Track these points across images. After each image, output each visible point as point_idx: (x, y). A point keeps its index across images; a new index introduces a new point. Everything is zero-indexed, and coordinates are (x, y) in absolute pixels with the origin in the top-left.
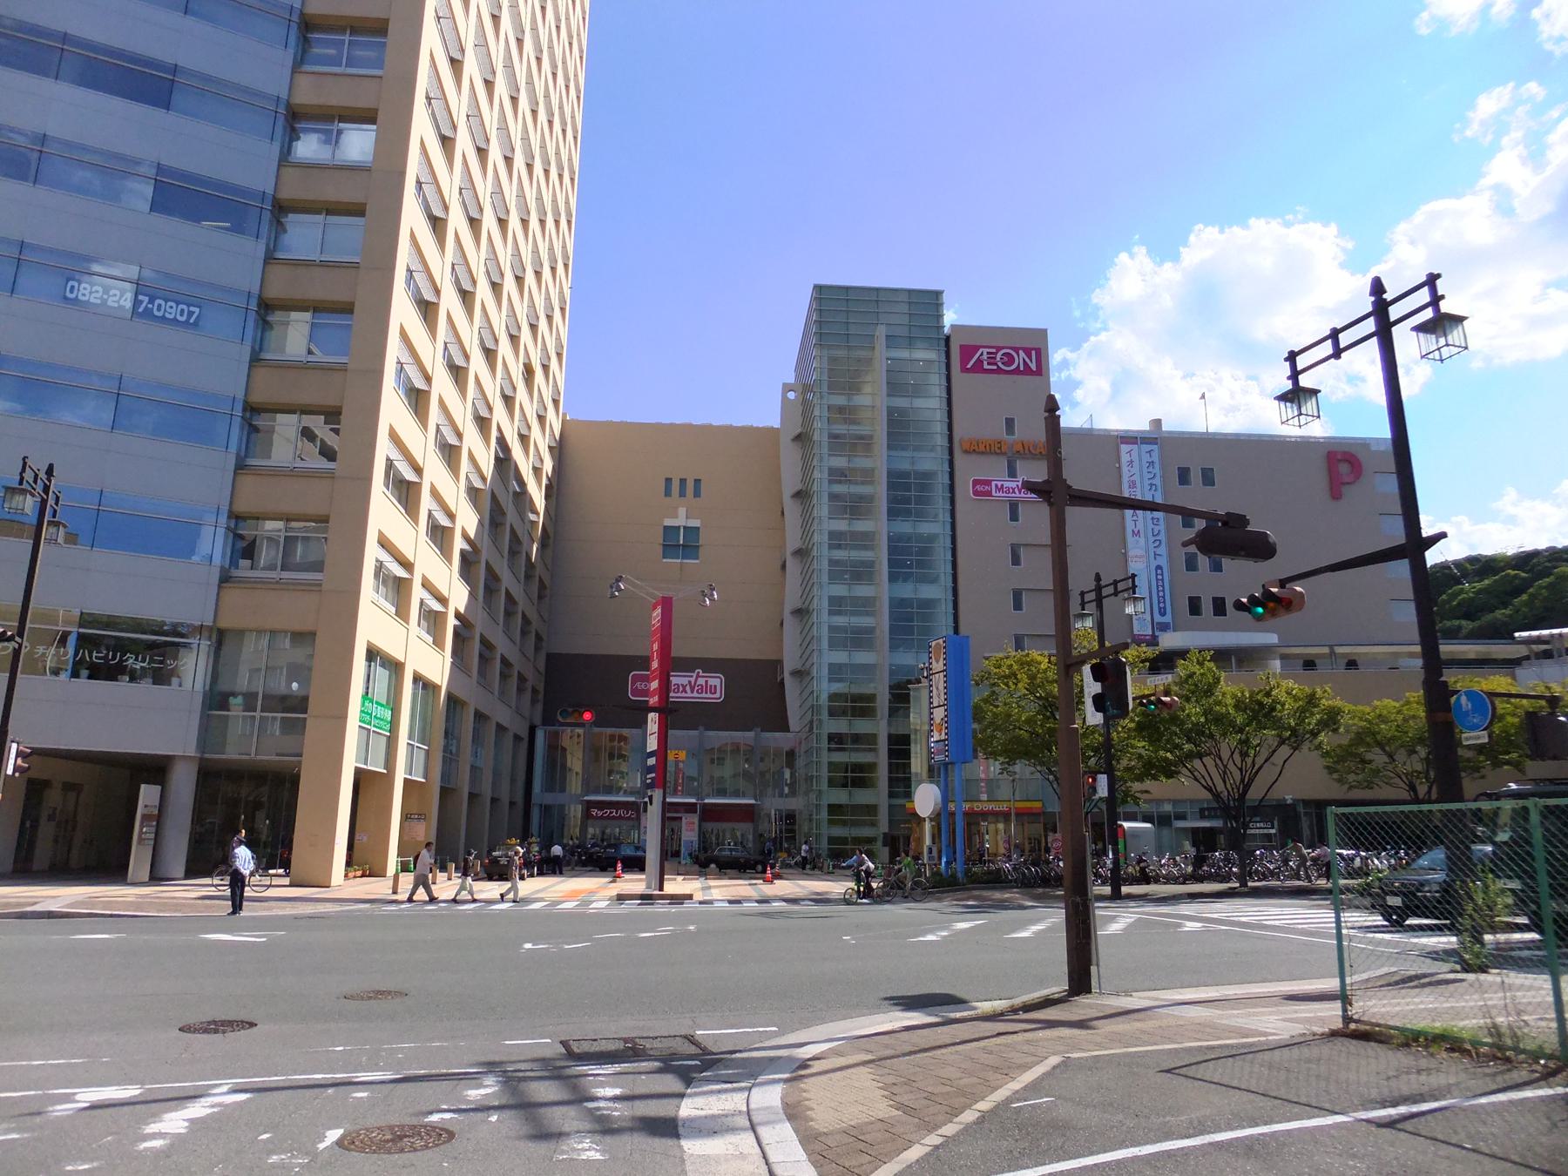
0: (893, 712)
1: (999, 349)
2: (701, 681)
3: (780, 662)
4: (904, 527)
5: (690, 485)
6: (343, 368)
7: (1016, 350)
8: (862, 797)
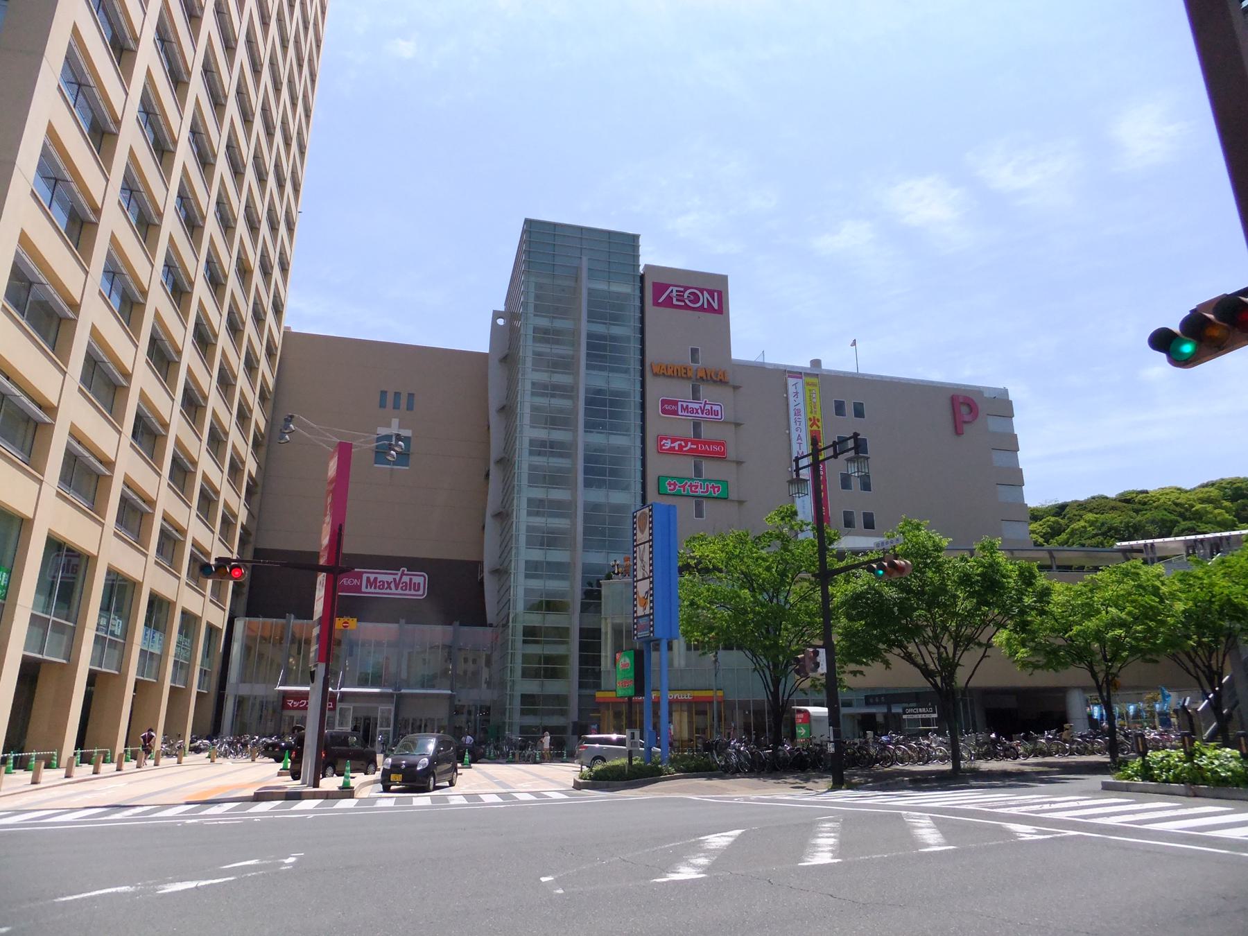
0: (585, 608)
1: (687, 288)
3: (481, 563)
7: (702, 291)
8: (554, 687)
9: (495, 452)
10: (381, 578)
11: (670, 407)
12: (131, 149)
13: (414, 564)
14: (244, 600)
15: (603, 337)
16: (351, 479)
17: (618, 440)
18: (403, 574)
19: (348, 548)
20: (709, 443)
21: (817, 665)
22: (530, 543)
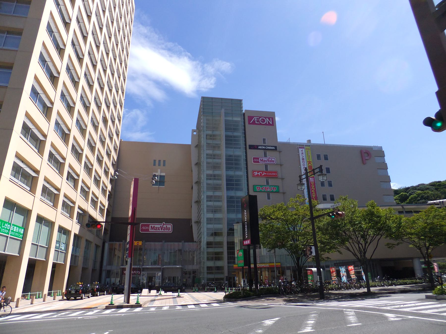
1: (260, 117)
2: (165, 226)
4: (231, 173)
7: (266, 118)
8: (219, 263)
9: (195, 179)
10: (156, 226)
11: (256, 160)
12: (64, 82)
13: (167, 221)
14: (108, 236)
15: (231, 137)
16: (138, 191)
17: (238, 173)
18: (164, 224)
19: (138, 216)
20: (271, 172)
21: (311, 252)
22: (208, 211)
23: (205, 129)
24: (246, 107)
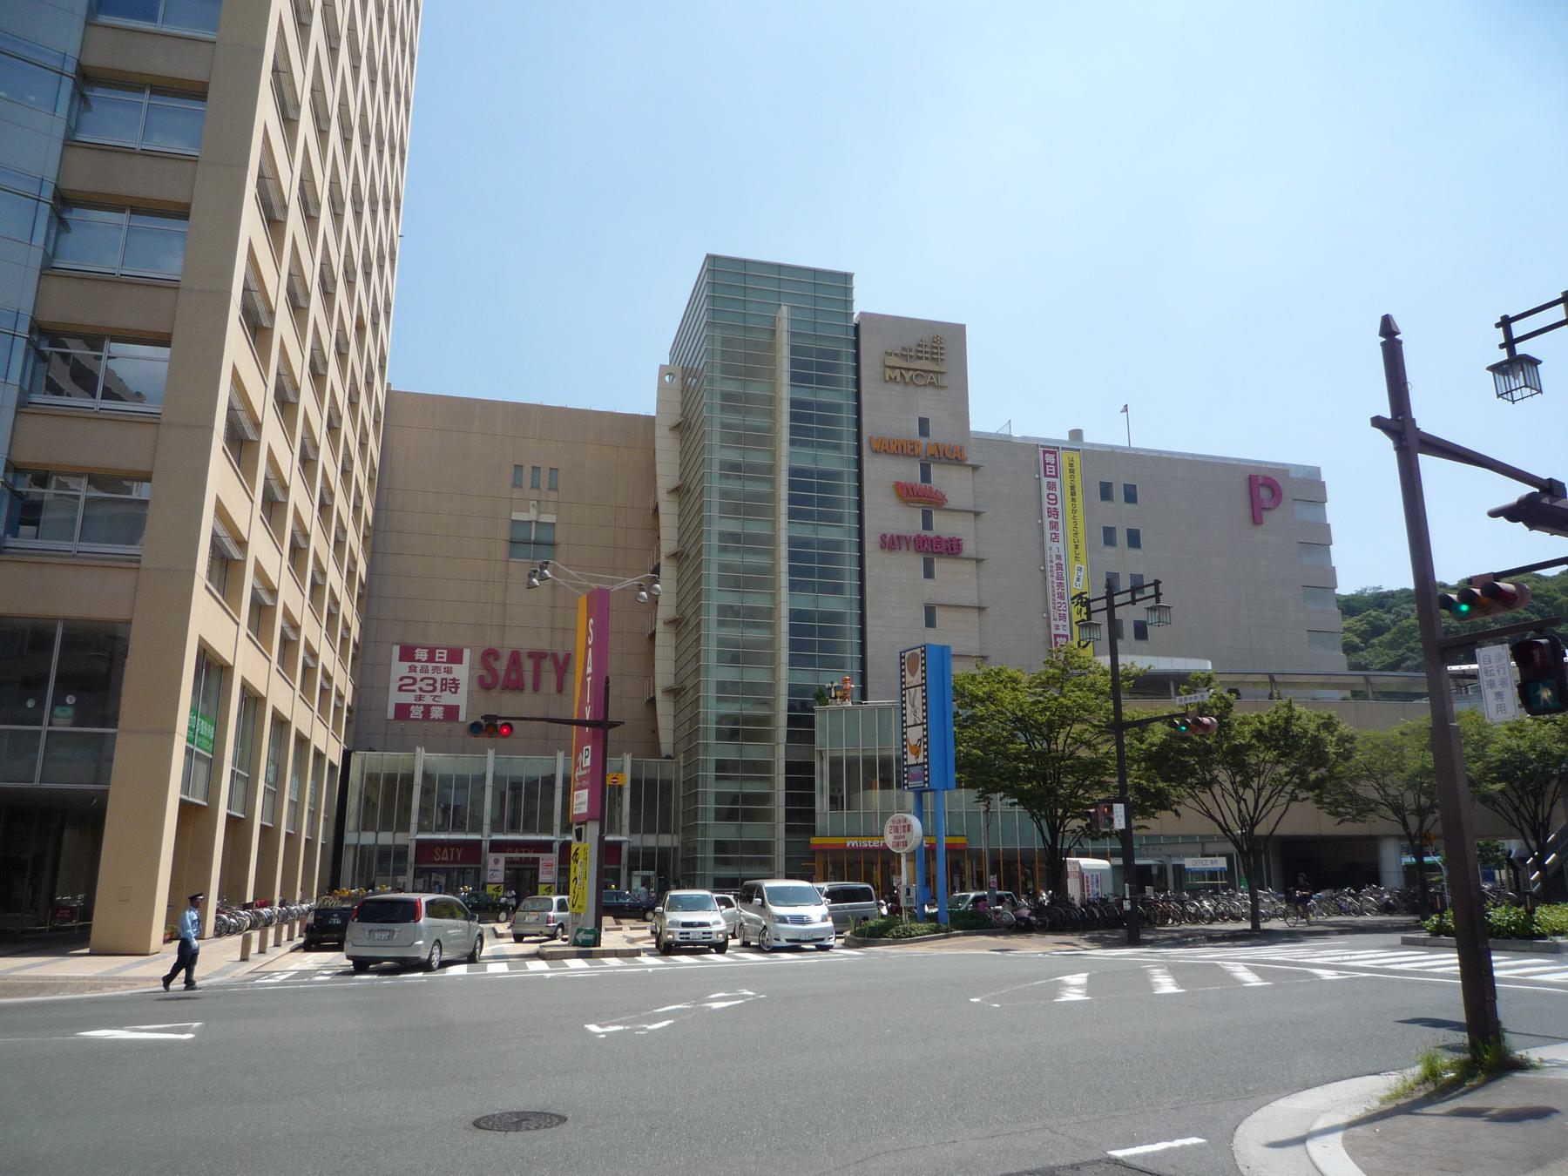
5: (544, 475)
6: (193, 160)
17: (829, 533)
23: (717, 374)
24: (865, 302)
